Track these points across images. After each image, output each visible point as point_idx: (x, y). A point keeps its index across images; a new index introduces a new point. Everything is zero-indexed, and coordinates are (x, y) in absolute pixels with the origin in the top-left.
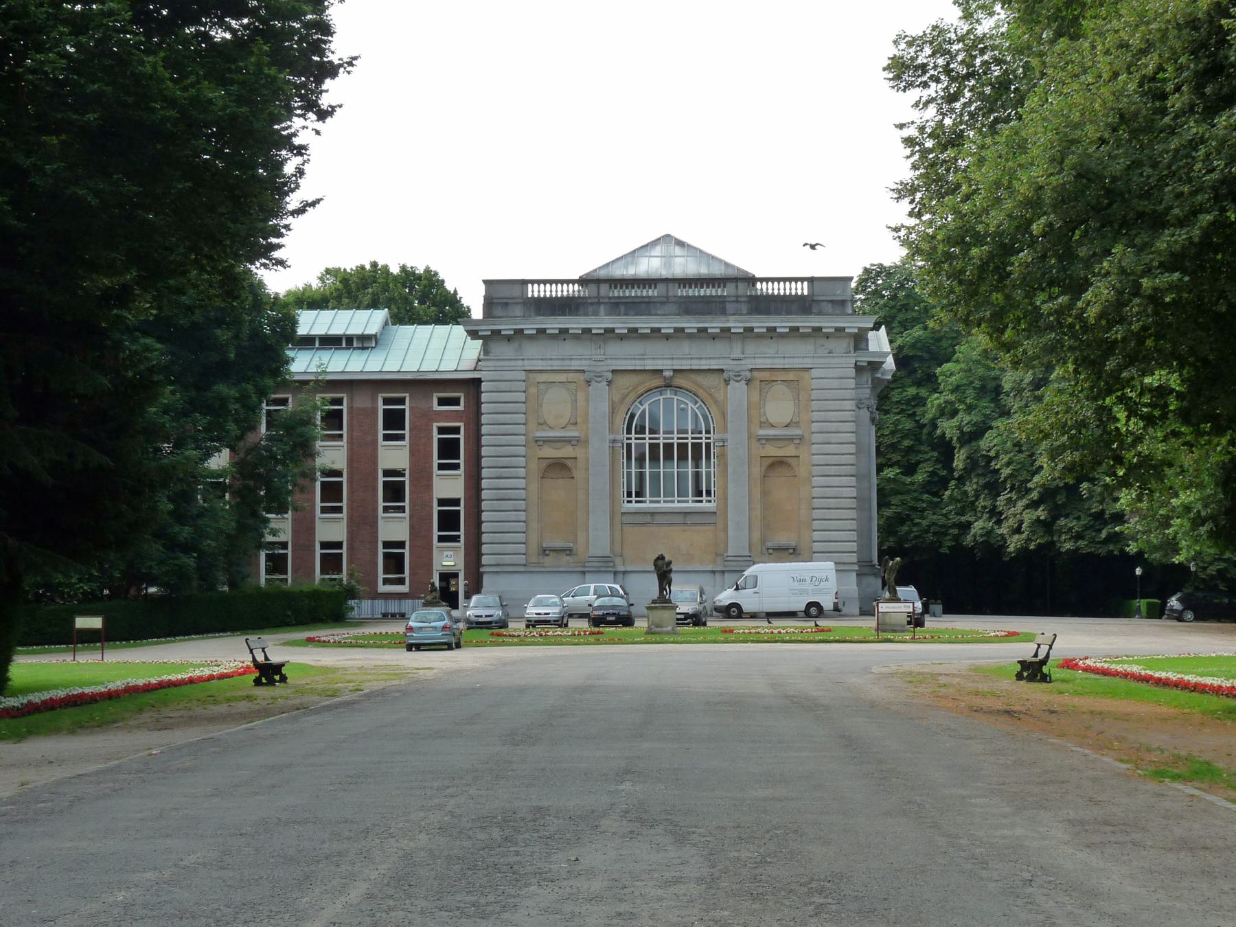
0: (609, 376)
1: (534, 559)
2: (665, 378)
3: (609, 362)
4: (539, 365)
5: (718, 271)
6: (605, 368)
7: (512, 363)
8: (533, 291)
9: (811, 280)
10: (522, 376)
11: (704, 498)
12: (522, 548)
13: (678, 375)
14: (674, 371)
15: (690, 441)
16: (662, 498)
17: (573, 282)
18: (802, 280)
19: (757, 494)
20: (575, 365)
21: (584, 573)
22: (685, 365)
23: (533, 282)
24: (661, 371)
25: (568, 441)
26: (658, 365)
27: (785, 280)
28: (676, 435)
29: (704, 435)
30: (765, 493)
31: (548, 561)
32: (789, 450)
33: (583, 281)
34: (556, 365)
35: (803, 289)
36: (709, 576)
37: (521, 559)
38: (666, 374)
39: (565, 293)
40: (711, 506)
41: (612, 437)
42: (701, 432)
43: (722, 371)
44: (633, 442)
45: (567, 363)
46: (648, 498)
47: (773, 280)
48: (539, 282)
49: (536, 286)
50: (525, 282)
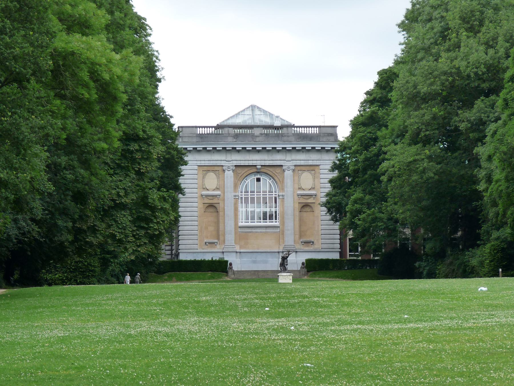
0: (293, 168)
2: (257, 169)
5: (277, 123)
6: (232, 165)
8: (200, 131)
9: (320, 127)
11: (274, 220)
13: (263, 167)
14: (262, 166)
16: (268, 220)
17: (212, 127)
18: (316, 127)
19: (297, 219)
21: (223, 252)
22: (267, 163)
23: (200, 127)
24: (256, 166)
25: (311, 196)
26: (254, 163)
27: (304, 127)
29: (274, 193)
30: (301, 220)
33: (218, 127)
35: (316, 131)
36: (235, 254)
38: (224, 168)
39: (303, 132)
40: (277, 224)
42: (254, 192)
43: (282, 166)
44: (243, 196)
46: (256, 221)
47: (302, 127)
48: (202, 127)
49: (310, 128)
50: (196, 127)
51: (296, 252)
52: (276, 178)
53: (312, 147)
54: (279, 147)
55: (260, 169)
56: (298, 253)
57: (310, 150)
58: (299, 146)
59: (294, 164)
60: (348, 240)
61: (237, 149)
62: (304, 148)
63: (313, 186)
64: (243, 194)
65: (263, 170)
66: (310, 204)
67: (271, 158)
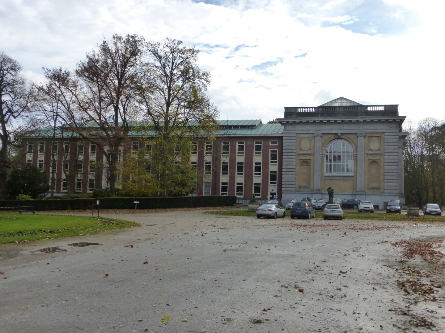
1: (297, 189)
2: (338, 136)
3: (321, 131)
4: (300, 132)
7: (292, 131)
10: (295, 135)
12: (294, 186)
15: (341, 155)
18: (313, 107)
20: (311, 132)
23: (299, 108)
28: (341, 153)
31: (302, 190)
32: (308, 157)
34: (305, 132)
35: (382, 109)
37: (294, 189)
41: (322, 153)
44: (328, 155)
45: (308, 131)
51: (366, 195)
52: (349, 140)
53: (286, 122)
54: (354, 119)
55: (340, 136)
56: (367, 196)
57: (347, 122)
58: (347, 119)
59: (365, 132)
60: (58, 150)
61: (382, 121)
62: (350, 121)
63: (380, 148)
64: (350, 155)
65: (342, 137)
66: (377, 161)
67: (348, 128)
